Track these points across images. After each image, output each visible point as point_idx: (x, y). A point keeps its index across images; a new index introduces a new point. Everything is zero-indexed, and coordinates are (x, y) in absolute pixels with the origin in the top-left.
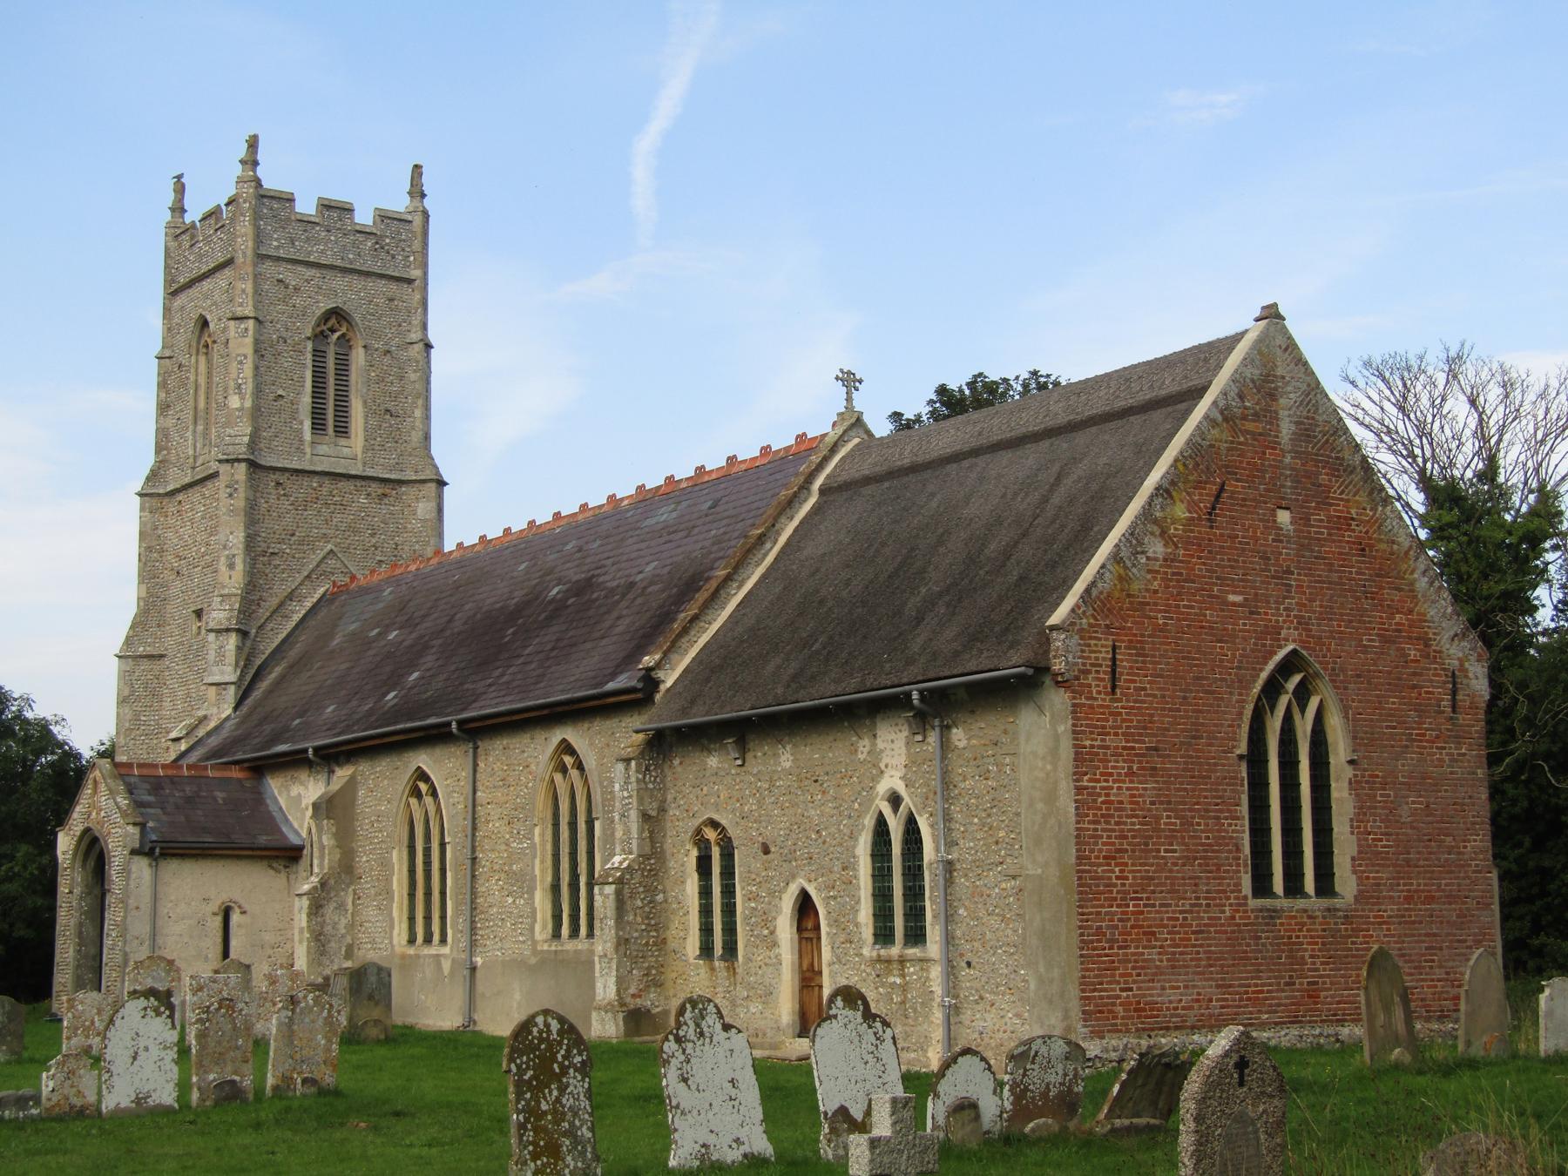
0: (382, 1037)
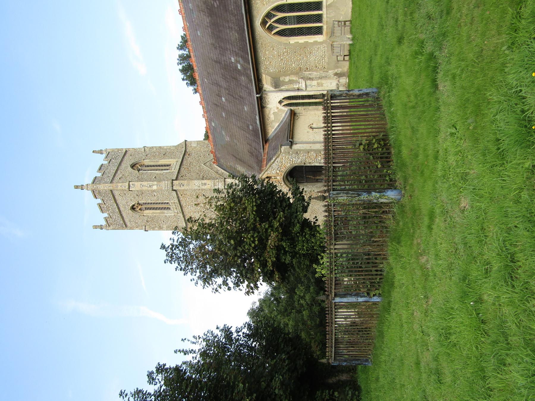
0: (322, 292)
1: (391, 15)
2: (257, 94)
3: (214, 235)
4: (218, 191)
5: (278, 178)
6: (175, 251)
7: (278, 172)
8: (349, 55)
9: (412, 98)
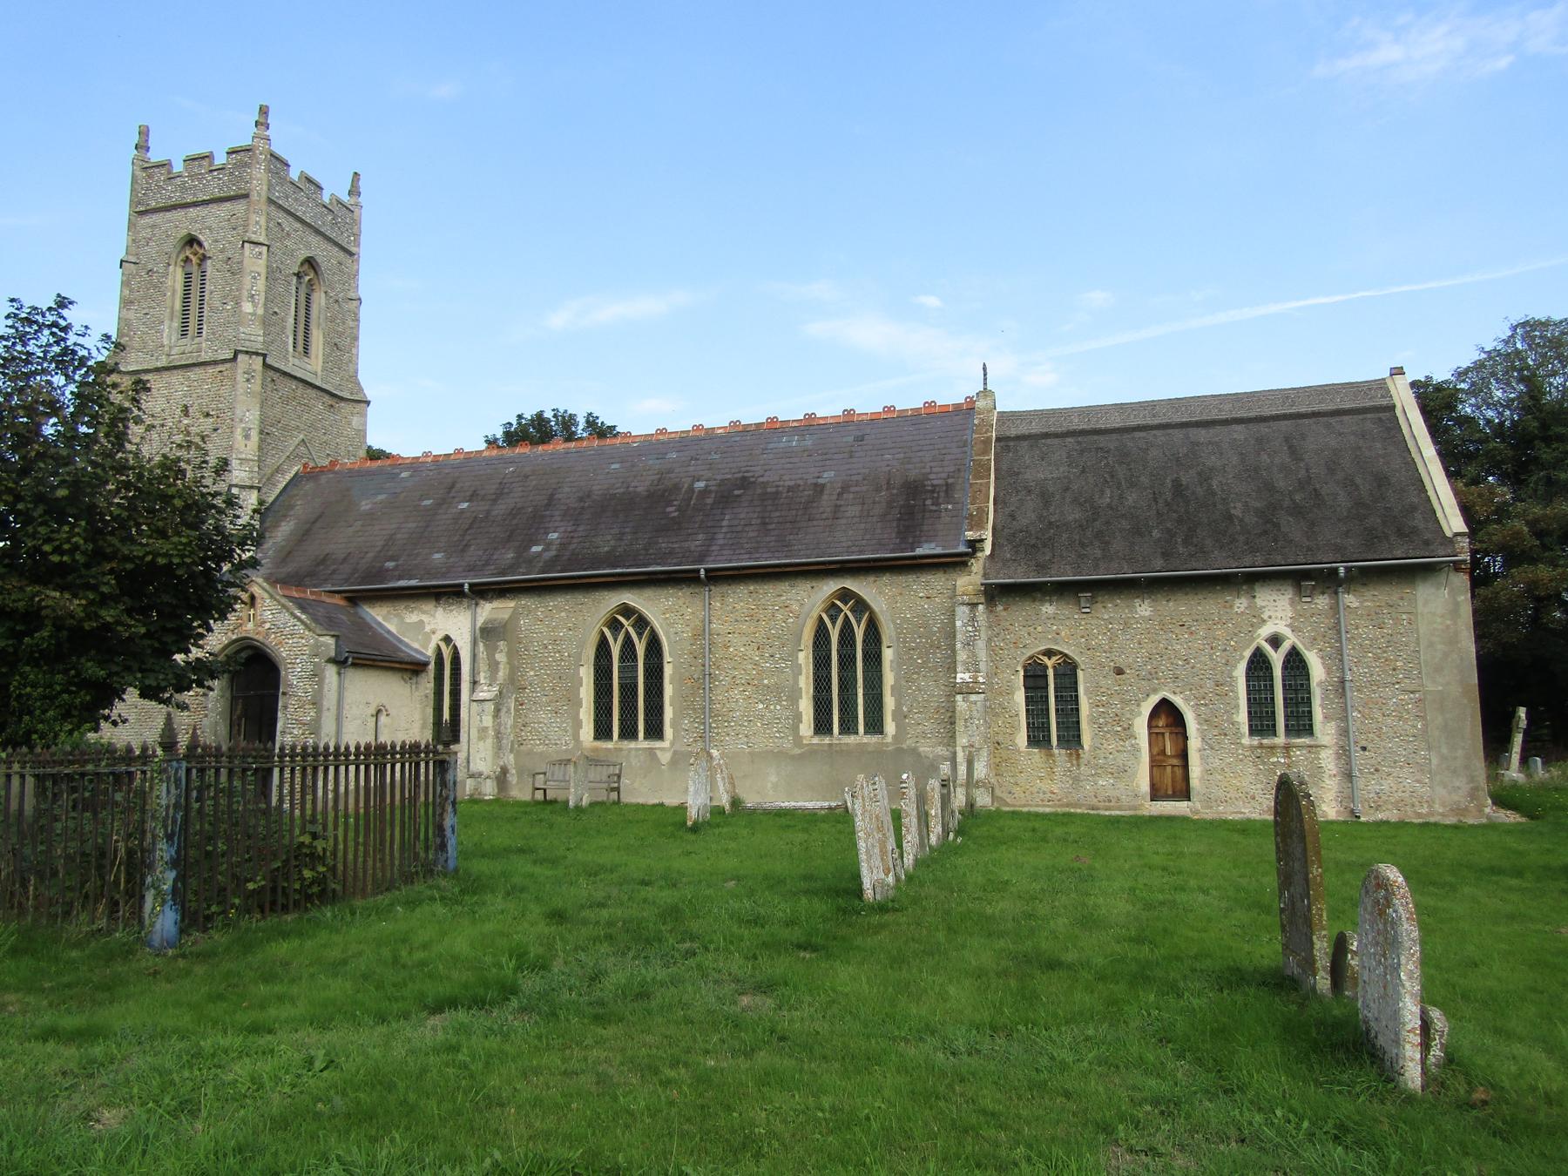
1: (615, 892)
2: (471, 585)
3: (87, 447)
4: (223, 466)
5: (250, 625)
6: (46, 332)
7: (267, 626)
8: (546, 802)
9: (419, 955)
